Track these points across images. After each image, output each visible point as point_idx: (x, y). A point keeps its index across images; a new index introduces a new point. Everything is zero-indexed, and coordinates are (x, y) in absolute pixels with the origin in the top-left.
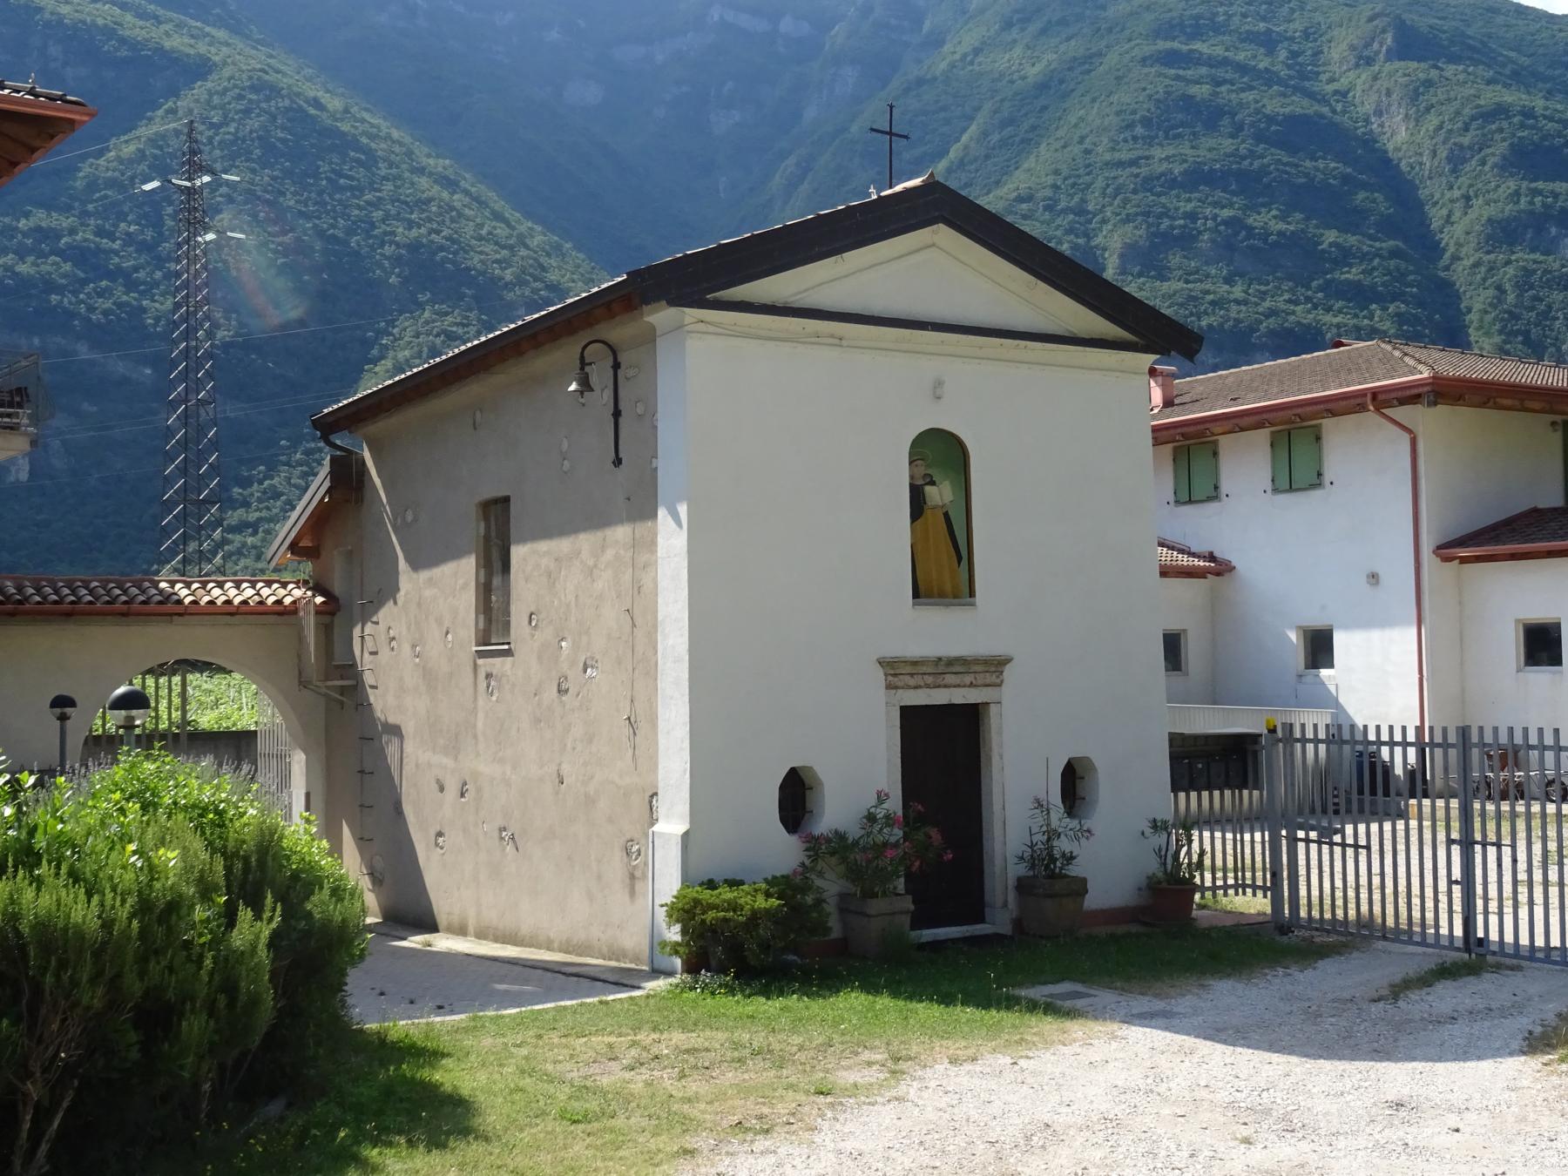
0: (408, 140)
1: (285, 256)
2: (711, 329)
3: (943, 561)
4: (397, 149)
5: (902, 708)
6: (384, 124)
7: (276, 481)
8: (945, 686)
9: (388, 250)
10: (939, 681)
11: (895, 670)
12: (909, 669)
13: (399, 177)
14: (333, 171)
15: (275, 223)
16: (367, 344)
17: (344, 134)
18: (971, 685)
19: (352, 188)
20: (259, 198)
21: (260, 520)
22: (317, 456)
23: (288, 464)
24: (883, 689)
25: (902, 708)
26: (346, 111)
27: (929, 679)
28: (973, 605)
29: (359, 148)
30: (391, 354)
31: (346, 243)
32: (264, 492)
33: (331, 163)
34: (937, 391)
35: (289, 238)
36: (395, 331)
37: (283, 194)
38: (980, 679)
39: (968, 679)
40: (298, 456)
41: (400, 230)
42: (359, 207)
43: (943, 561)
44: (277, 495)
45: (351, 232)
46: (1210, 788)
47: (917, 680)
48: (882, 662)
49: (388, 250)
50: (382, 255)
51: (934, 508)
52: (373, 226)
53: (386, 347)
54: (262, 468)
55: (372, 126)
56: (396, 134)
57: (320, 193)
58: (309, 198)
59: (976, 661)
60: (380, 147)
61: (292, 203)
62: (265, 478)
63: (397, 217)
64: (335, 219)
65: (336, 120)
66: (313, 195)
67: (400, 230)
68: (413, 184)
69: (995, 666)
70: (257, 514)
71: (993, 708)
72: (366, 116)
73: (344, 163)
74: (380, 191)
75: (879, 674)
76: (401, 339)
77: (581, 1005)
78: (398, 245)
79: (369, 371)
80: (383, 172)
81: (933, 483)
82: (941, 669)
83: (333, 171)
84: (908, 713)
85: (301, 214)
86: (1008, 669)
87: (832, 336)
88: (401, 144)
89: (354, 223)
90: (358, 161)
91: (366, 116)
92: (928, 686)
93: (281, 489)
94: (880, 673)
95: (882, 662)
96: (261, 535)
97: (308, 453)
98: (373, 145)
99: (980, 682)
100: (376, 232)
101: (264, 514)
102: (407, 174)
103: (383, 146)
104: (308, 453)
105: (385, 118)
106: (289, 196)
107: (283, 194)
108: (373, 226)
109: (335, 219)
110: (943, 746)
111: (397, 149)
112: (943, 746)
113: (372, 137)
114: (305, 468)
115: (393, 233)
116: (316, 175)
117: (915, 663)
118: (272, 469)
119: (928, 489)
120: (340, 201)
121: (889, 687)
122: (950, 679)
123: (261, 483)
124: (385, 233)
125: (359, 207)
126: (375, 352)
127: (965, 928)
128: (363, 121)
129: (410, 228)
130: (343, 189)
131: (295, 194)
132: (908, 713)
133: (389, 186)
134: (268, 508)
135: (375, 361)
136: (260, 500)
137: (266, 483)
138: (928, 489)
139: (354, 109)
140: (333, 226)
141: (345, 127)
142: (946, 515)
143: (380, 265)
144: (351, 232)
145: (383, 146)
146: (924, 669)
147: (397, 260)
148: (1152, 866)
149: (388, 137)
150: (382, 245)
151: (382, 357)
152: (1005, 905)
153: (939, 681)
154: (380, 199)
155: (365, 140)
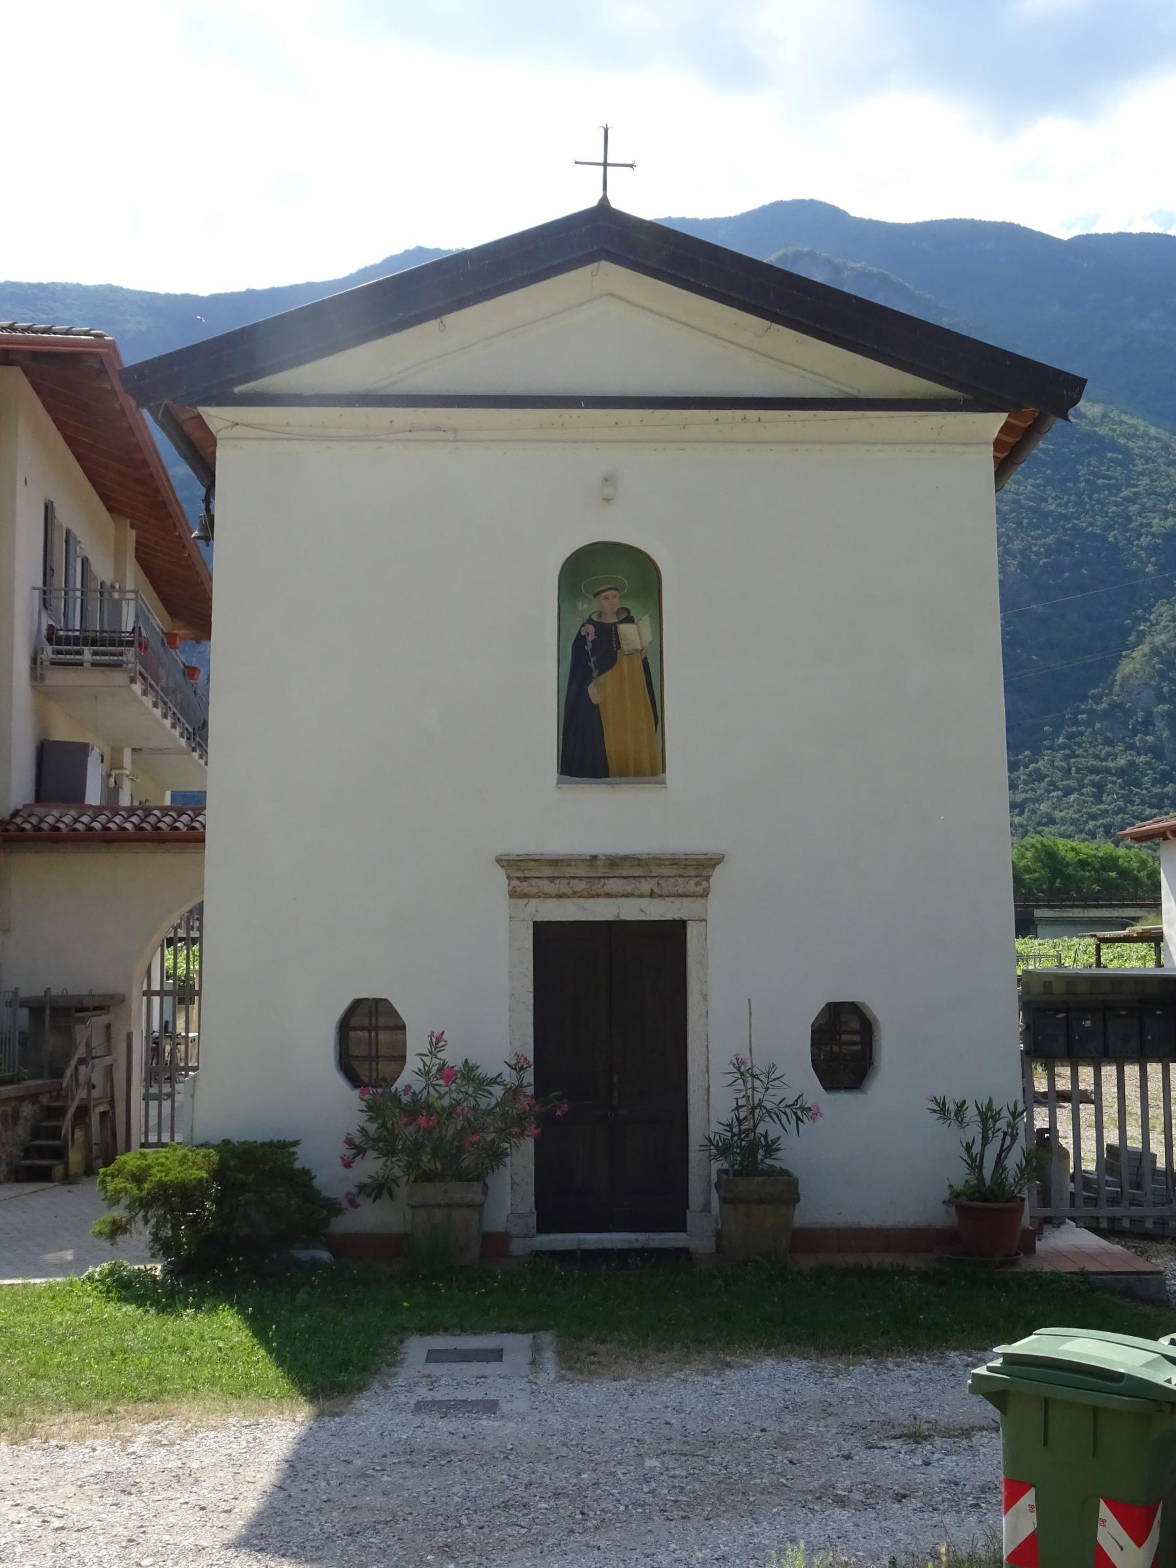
0: (1165, 435)
1: (1048, 556)
2: (262, 434)
3: (603, 720)
4: (1154, 444)
5: (536, 925)
6: (1141, 424)
7: (1040, 764)
8: (609, 895)
9: (1144, 541)
10: (597, 887)
11: (524, 872)
12: (547, 871)
13: (1156, 471)
14: (1091, 473)
15: (1037, 527)
16: (1125, 632)
17: (1103, 437)
18: (652, 894)
19: (1108, 487)
20: (1022, 506)
21: (1025, 800)
22: (1078, 739)
23: (1051, 748)
24: (504, 900)
25: (536, 925)
26: (1105, 416)
27: (580, 886)
28: (663, 782)
29: (1115, 448)
30: (1148, 639)
31: (1103, 538)
32: (1030, 775)
33: (1089, 465)
34: (608, 491)
35: (1051, 540)
36: (1152, 617)
37: (1045, 500)
38: (667, 887)
39: (645, 886)
40: (1061, 740)
41: (1157, 521)
42: (1117, 504)
43: (603, 720)
44: (1041, 777)
45: (1108, 528)
46: (1142, 1059)
47: (562, 886)
48: (504, 862)
49: (1144, 541)
50: (1139, 546)
51: (631, 653)
52: (1129, 519)
53: (1143, 633)
54: (1027, 753)
55: (1130, 426)
56: (1153, 431)
57: (1080, 494)
58: (1069, 501)
59: (656, 861)
60: (1137, 446)
61: (1053, 507)
62: (1031, 762)
63: (1154, 509)
64: (1093, 517)
65: (1095, 426)
66: (1073, 498)
67: (1157, 521)
68: (1169, 476)
69: (698, 869)
70: (1023, 796)
71: (692, 931)
72: (1125, 418)
73: (1102, 464)
74: (1136, 486)
75: (500, 877)
76: (1158, 624)
77: (25, 1286)
78: (1154, 536)
79: (1126, 656)
80: (1140, 468)
81: (630, 620)
82: (601, 871)
83: (1091, 473)
84: (544, 933)
85: (1061, 516)
86: (718, 874)
87: (438, 429)
88: (1157, 439)
89: (1112, 519)
90: (1115, 461)
91: (1125, 418)
92: (580, 895)
93: (1045, 771)
94: (500, 875)
95: (504, 862)
96: (1026, 814)
97: (1070, 736)
98: (1130, 444)
99: (665, 891)
100: (1132, 525)
101: (1029, 795)
102: (1163, 467)
103: (1140, 443)
104: (1070, 736)
105: (1144, 418)
106: (1050, 501)
107: (1045, 500)
108: (1129, 519)
109: (1093, 517)
110: (611, 985)
111: (1154, 444)
112: (611, 985)
113: (1129, 437)
114: (1067, 752)
115: (1150, 525)
116: (1076, 480)
117: (554, 862)
118: (1037, 753)
119: (623, 628)
120: (1099, 501)
121: (513, 894)
122: (612, 885)
123: (1026, 767)
124: (1142, 525)
125: (1117, 504)
126: (1132, 638)
127: (631, 1236)
128: (1121, 423)
129: (1166, 519)
130: (1100, 489)
131: (1055, 499)
132: (544, 933)
133: (1146, 480)
134: (1033, 790)
135: (1133, 647)
136: (1026, 783)
137: (1032, 766)
138: (623, 628)
139: (1114, 414)
140: (1091, 524)
141: (1102, 431)
142: (645, 662)
143: (1136, 556)
144: (1108, 528)
145: (1140, 443)
146: (573, 871)
147: (1154, 550)
148: (960, 1175)
149: (1146, 434)
150: (1138, 537)
151: (1139, 642)
152: (706, 1208)
153: (597, 887)
154: (1135, 493)
155: (1122, 441)
